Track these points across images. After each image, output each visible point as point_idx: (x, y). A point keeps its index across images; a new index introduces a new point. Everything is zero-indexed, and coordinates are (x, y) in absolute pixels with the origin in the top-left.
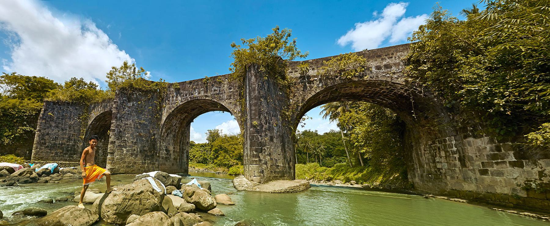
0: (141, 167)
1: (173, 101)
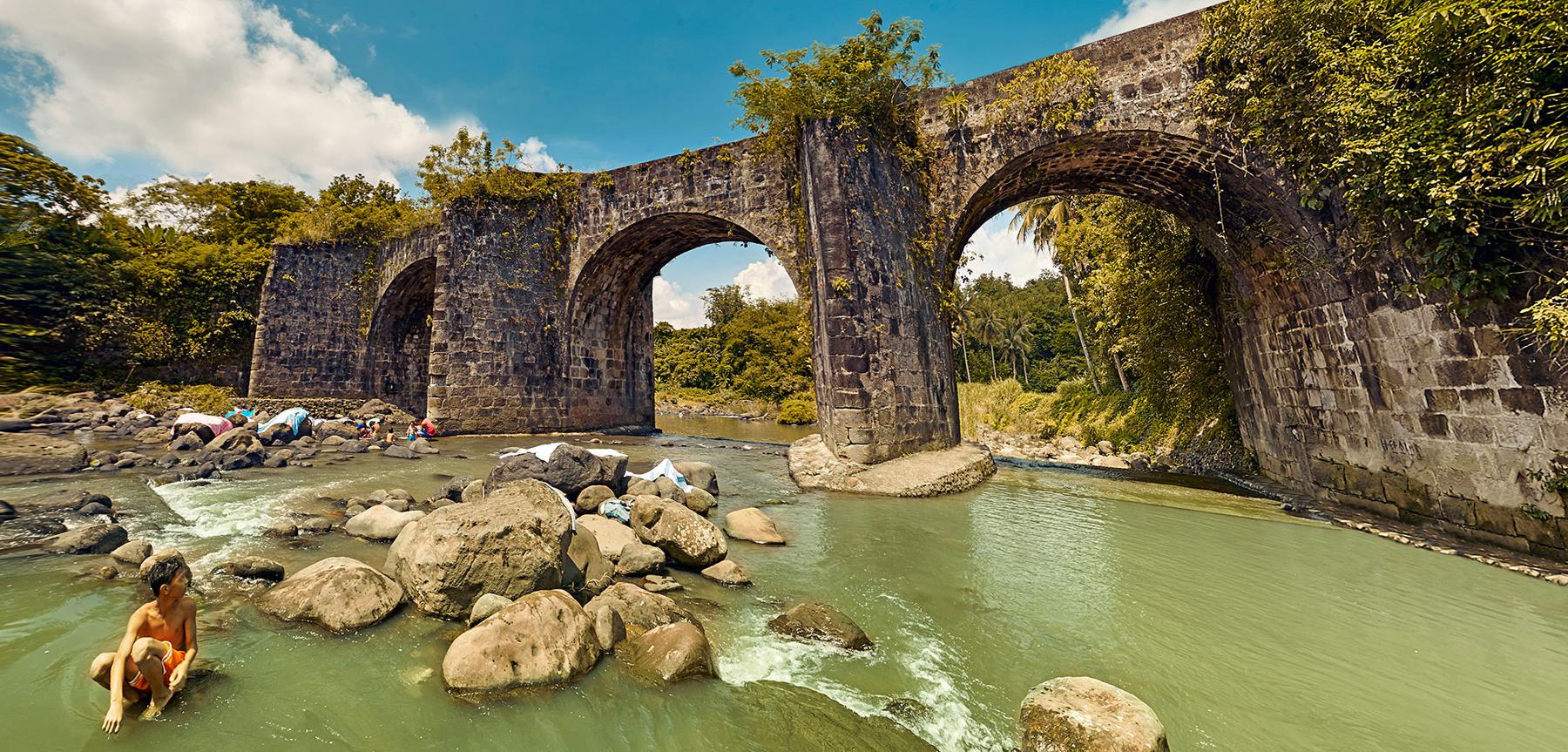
0: (519, 413)
1: (596, 222)
